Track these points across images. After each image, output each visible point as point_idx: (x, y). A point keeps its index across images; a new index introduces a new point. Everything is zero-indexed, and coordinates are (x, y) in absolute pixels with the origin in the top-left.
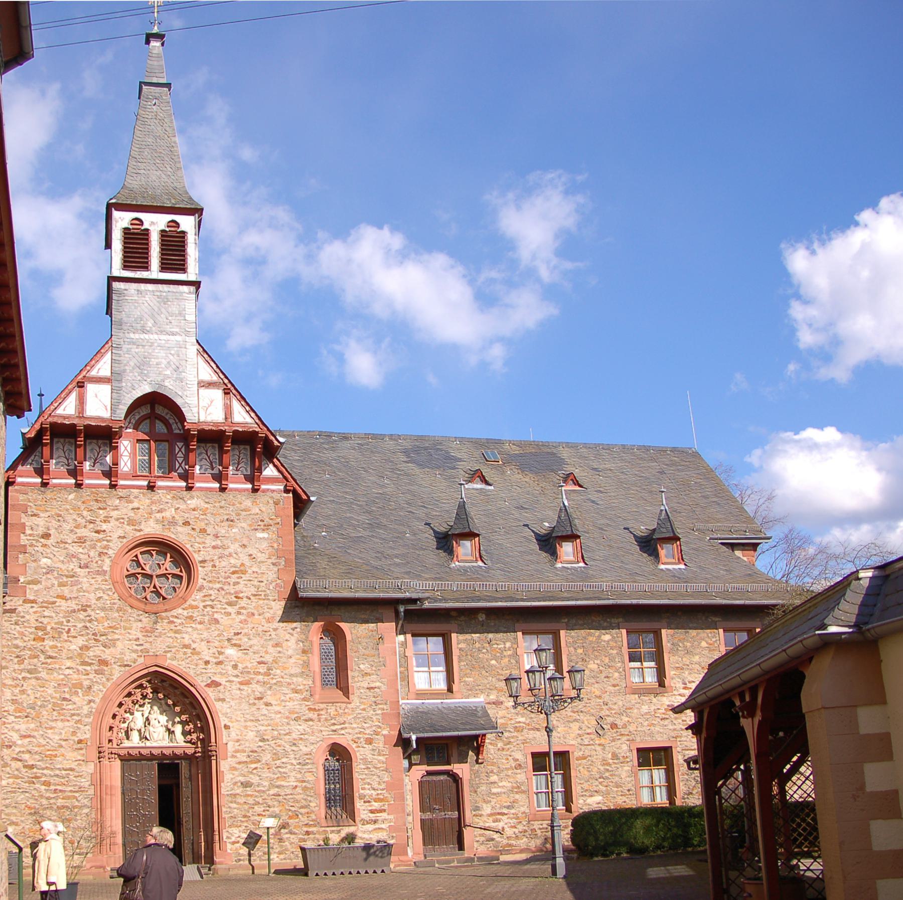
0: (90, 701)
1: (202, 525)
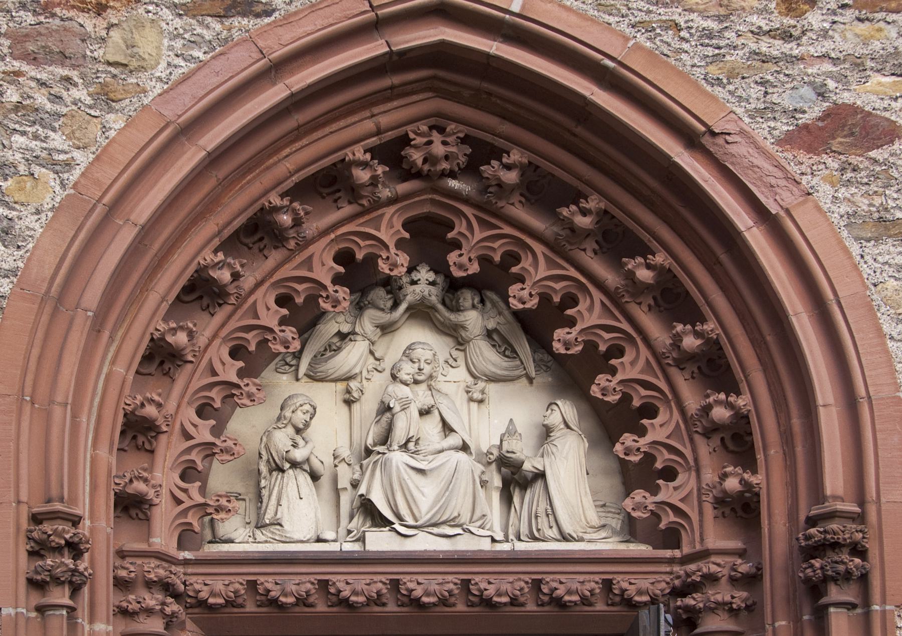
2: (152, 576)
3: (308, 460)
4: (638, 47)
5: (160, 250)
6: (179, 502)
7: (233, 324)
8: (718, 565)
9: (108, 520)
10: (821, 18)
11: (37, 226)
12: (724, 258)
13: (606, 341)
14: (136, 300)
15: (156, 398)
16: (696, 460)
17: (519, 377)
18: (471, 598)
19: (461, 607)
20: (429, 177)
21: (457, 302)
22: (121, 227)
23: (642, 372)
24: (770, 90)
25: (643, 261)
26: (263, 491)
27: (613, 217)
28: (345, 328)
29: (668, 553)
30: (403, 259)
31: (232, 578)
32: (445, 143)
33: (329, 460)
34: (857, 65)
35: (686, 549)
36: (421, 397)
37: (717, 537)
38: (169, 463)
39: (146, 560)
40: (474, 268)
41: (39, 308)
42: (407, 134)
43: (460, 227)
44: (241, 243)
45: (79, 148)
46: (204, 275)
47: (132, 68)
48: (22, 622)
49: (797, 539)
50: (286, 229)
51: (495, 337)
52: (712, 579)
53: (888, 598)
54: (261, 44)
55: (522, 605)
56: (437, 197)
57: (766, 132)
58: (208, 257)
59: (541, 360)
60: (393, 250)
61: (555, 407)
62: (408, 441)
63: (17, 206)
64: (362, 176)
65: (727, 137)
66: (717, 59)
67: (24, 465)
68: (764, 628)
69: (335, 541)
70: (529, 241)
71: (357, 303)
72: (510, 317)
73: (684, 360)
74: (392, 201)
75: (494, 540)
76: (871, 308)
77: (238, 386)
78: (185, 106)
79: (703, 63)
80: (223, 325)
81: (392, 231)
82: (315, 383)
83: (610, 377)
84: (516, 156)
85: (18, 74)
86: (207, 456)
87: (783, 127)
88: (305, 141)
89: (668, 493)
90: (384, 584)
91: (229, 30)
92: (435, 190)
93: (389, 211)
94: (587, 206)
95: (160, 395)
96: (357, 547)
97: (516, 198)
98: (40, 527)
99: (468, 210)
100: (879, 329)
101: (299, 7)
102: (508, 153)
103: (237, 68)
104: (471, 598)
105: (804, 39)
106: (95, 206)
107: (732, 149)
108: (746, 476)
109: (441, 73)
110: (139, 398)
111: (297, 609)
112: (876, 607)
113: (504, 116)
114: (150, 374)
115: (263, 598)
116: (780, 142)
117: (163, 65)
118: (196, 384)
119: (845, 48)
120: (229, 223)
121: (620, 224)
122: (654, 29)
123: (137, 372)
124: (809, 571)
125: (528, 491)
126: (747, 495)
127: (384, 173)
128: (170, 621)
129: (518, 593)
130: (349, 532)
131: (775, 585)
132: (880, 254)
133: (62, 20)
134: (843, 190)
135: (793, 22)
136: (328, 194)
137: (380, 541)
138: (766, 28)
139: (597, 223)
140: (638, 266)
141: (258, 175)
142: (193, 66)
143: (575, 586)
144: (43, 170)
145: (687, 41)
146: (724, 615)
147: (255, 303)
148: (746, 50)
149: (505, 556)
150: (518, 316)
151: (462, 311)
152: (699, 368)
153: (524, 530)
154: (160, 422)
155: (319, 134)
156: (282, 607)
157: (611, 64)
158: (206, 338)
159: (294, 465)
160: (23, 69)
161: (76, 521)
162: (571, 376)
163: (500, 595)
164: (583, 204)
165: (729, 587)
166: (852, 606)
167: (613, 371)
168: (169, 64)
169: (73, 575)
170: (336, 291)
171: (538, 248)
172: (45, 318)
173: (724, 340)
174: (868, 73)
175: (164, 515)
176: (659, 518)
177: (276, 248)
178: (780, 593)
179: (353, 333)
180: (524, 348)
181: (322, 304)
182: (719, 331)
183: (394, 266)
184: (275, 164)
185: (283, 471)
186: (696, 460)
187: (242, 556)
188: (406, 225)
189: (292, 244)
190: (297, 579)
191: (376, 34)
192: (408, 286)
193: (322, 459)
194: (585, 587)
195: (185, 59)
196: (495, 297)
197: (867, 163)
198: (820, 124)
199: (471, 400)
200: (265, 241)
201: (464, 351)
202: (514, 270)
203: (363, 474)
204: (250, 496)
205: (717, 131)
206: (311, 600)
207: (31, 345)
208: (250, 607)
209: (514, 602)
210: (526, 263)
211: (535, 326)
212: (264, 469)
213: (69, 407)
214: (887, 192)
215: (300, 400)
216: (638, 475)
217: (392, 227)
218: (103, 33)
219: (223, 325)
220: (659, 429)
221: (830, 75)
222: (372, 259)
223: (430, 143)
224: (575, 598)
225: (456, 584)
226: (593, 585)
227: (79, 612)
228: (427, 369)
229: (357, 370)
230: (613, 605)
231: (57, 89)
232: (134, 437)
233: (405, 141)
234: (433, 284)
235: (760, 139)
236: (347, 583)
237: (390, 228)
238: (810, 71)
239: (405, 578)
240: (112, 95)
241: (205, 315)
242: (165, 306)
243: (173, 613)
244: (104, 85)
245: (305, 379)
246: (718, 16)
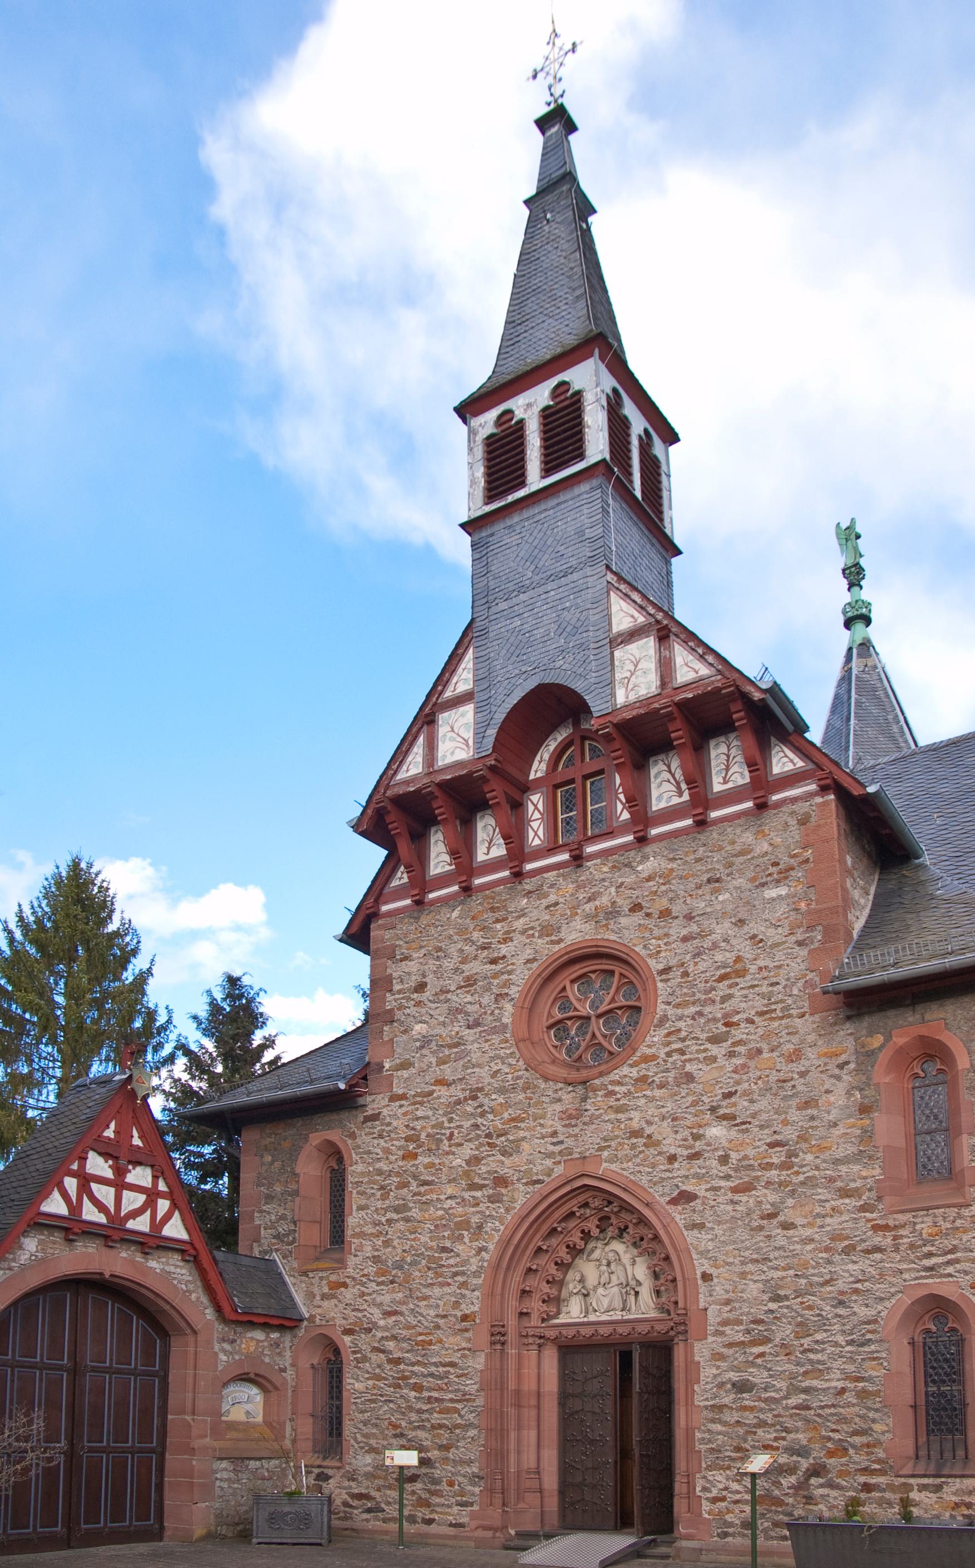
1: (664, 903)
4: (631, 1180)
123: (251, 1523)
172: (512, 1374)
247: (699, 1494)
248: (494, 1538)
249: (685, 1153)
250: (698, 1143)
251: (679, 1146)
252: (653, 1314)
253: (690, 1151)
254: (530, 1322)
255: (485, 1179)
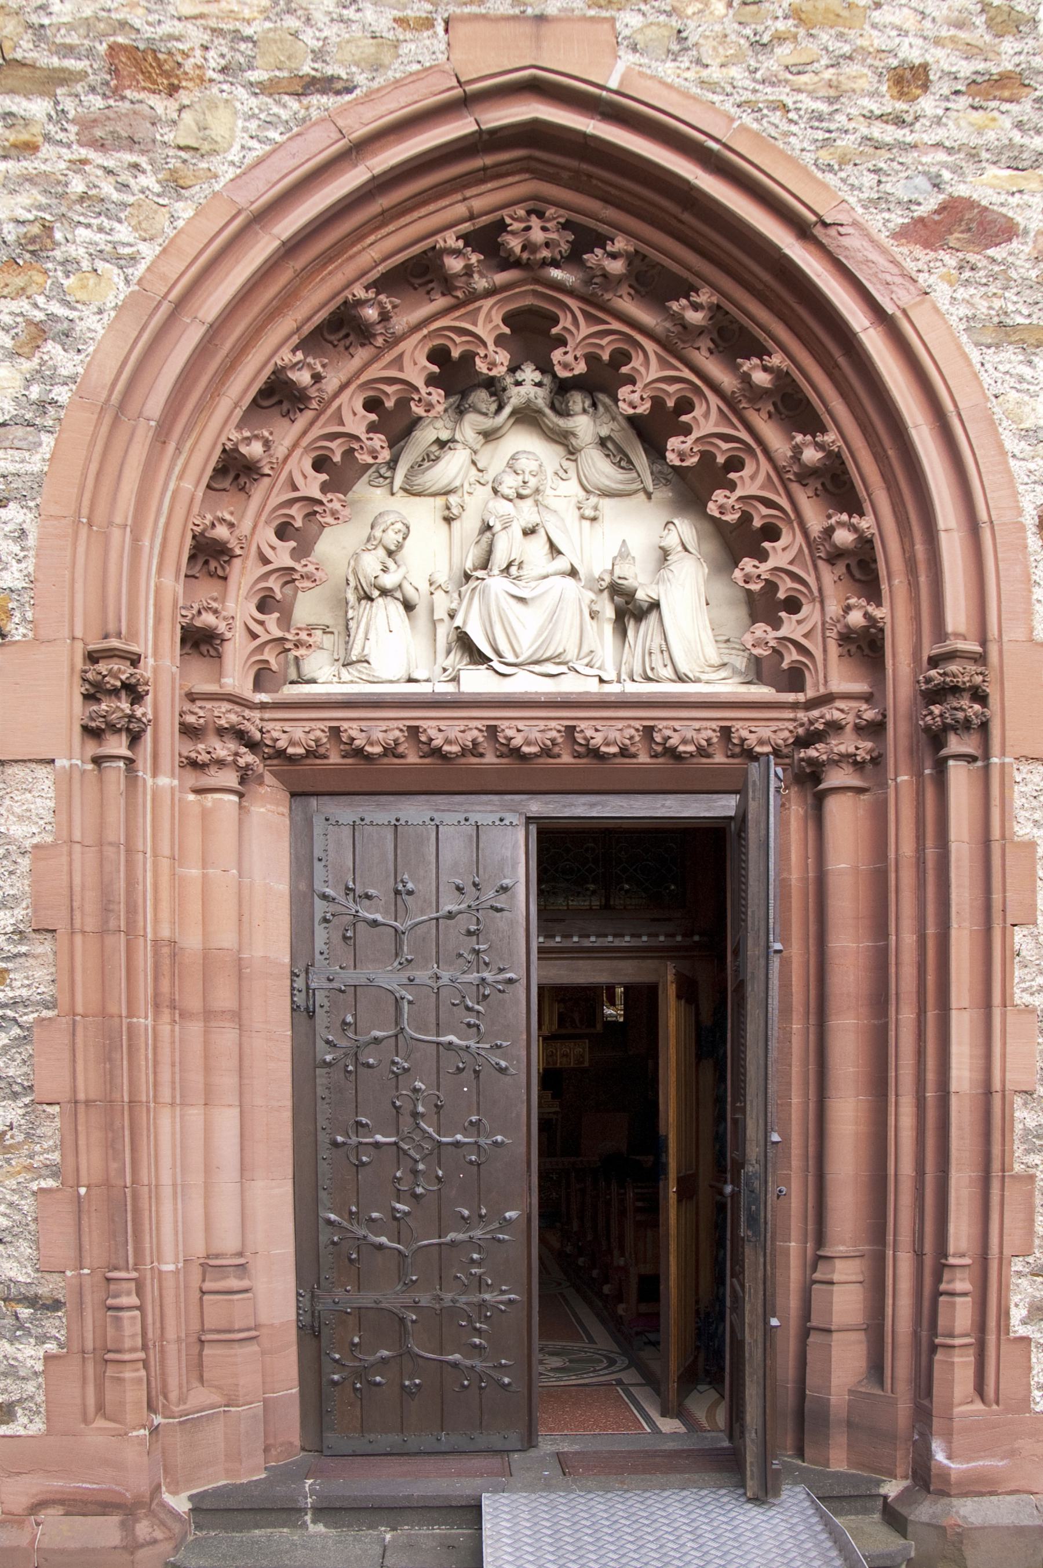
0: (38, 333)
2: (223, 722)
3: (400, 586)
4: (743, 128)
5: (231, 350)
6: (254, 636)
7: (316, 431)
8: (842, 711)
9: (173, 658)
10: (934, 103)
11: (98, 327)
12: (842, 361)
13: (724, 452)
14: (206, 405)
15: (228, 517)
16: (820, 590)
17: (636, 492)
18: (576, 747)
19: (566, 759)
20: (529, 266)
21: (567, 405)
22: (188, 325)
23: (762, 488)
24: (883, 179)
25: (758, 362)
26: (351, 623)
27: (727, 313)
28: (445, 436)
29: (791, 697)
30: (503, 357)
31: (313, 724)
32: (544, 229)
33: (424, 587)
34: (973, 156)
35: (810, 693)
36: (526, 513)
37: (839, 677)
38: (243, 592)
39: (216, 704)
40: (581, 368)
41: (99, 418)
42: (503, 219)
43: (565, 321)
44: (326, 340)
45: (145, 240)
46: (282, 377)
47: (203, 152)
48: (76, 776)
49: (918, 682)
50: (373, 324)
51: (610, 445)
52: (835, 727)
53: (1008, 749)
54: (341, 123)
55: (634, 756)
56: (540, 289)
57: (880, 225)
58: (286, 356)
59: (660, 472)
60: (491, 347)
61: (671, 526)
62: (510, 565)
63: (79, 306)
64: (454, 265)
65: (840, 229)
66: (826, 143)
67: (79, 597)
68: (886, 783)
69: (428, 681)
70: (639, 337)
71: (458, 407)
72: (624, 423)
73: (806, 475)
74: (489, 293)
75: (602, 681)
76: (992, 423)
77: (321, 503)
78: (259, 191)
79: (813, 148)
80: (305, 433)
81: (490, 326)
82: (413, 498)
83: (727, 493)
84: (620, 244)
85: (84, 162)
86: (287, 583)
87: (898, 219)
88: (391, 228)
89: (791, 627)
90: (481, 731)
91: (307, 109)
92: (537, 281)
93: (488, 303)
94: (698, 300)
95: (232, 513)
96: (450, 688)
97: (624, 290)
98: (96, 666)
99: (573, 304)
100: (1000, 446)
101: (383, 83)
102: (612, 240)
103: (314, 150)
104: (576, 747)
105: (918, 126)
106: (160, 303)
107: (845, 241)
108: (870, 609)
109: (538, 154)
110: (209, 517)
111: (386, 760)
112: (995, 760)
113: (607, 200)
114: (224, 490)
115: (347, 747)
116: (895, 236)
117: (237, 147)
118: (275, 500)
119: (960, 136)
120: (309, 319)
121: (734, 321)
122: (760, 110)
123: (209, 487)
124: (929, 718)
125: (643, 623)
126: (873, 630)
127: (479, 261)
128: (245, 775)
129: (627, 742)
130: (445, 670)
131: (899, 734)
132: (1000, 362)
133: (132, 102)
134: (962, 290)
135: (905, 107)
136: (420, 285)
137: (477, 681)
138: (878, 112)
139: (711, 319)
140: (754, 367)
141: (341, 265)
142: (268, 148)
143: (690, 734)
144: (107, 265)
145: (796, 123)
146: (849, 769)
147: (340, 407)
148: (858, 135)
149: (613, 699)
150: (632, 420)
151: (569, 415)
152: (823, 484)
153: (638, 669)
154: (233, 544)
155: (408, 219)
156: (369, 758)
157: (715, 146)
158: (285, 447)
159: (384, 592)
160: (89, 157)
161: (135, 660)
162: (690, 489)
163: (608, 745)
164: (694, 298)
165: (854, 737)
166: (971, 759)
167: (732, 486)
168: (243, 147)
169: (130, 722)
170: (430, 394)
171: (650, 346)
172: (104, 429)
173: (846, 454)
174: (984, 164)
175: (237, 652)
176: (781, 656)
177: (363, 345)
178: (903, 743)
179: (453, 440)
180: (640, 459)
181: (414, 408)
182: (841, 443)
183: (492, 365)
184: (360, 252)
185: (372, 600)
186: (820, 590)
187: (324, 699)
188: (506, 320)
189: (380, 341)
190: (384, 725)
191: (465, 112)
192: (513, 387)
193: (417, 587)
194: (700, 736)
195: (259, 141)
196: (607, 400)
197: (985, 262)
198: (936, 217)
199: (583, 517)
200: (351, 338)
201: (575, 460)
202: (624, 370)
203: (460, 604)
204: (338, 629)
205: (828, 221)
206: (401, 749)
207: (88, 460)
208: (335, 758)
209: (624, 752)
210: (637, 362)
211: (652, 430)
212: (351, 597)
213: (128, 529)
214: (1007, 294)
215: (390, 519)
216: (766, 605)
217: (491, 321)
218: (175, 116)
219: (305, 433)
220: (782, 553)
221: (945, 165)
222: (468, 358)
223: (528, 229)
224: (691, 748)
225: (559, 731)
226: (710, 733)
227: (140, 764)
228: (533, 482)
229: (457, 483)
230: (733, 756)
231: (125, 177)
232: (206, 562)
233: (501, 226)
234: (539, 384)
235: (874, 232)
236: (440, 730)
237: (488, 323)
238: (924, 160)
239: (503, 724)
240: (181, 182)
241: (286, 422)
242: (239, 413)
243: (248, 765)
244: (173, 171)
245: (401, 493)
246: (828, 98)
247: (1019, 1330)
248: (132, 1546)
249: (965, 69)
250: (1008, 45)
251: (938, 42)
252: (728, 686)
253: (981, 66)
254: (219, 675)
255: (69, 50)
